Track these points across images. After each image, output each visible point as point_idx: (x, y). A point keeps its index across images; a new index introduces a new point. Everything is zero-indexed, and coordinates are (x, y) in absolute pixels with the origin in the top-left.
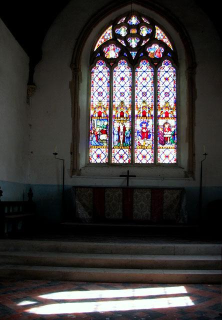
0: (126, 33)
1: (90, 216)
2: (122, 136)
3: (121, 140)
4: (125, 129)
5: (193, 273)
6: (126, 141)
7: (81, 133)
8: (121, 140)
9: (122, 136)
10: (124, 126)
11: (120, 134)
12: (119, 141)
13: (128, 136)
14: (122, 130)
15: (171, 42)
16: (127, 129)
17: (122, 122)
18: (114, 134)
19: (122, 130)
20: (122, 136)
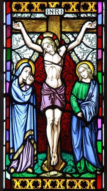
0: (40, 179)
1: (14, 181)
2: (58, 113)
3: (52, 137)
4: (69, 69)
5: (60, 126)
6: (76, 140)
7: (96, 92)
8: (52, 137)
9: (54, 116)
10: (68, 53)
11: (46, 101)
12: (38, 140)
13: (89, 111)
14: (53, 78)
15: (85, 19)
16: (84, 72)
17: (55, 28)
18: (11, 103)
19: (53, 78)
20: (54, 116)
